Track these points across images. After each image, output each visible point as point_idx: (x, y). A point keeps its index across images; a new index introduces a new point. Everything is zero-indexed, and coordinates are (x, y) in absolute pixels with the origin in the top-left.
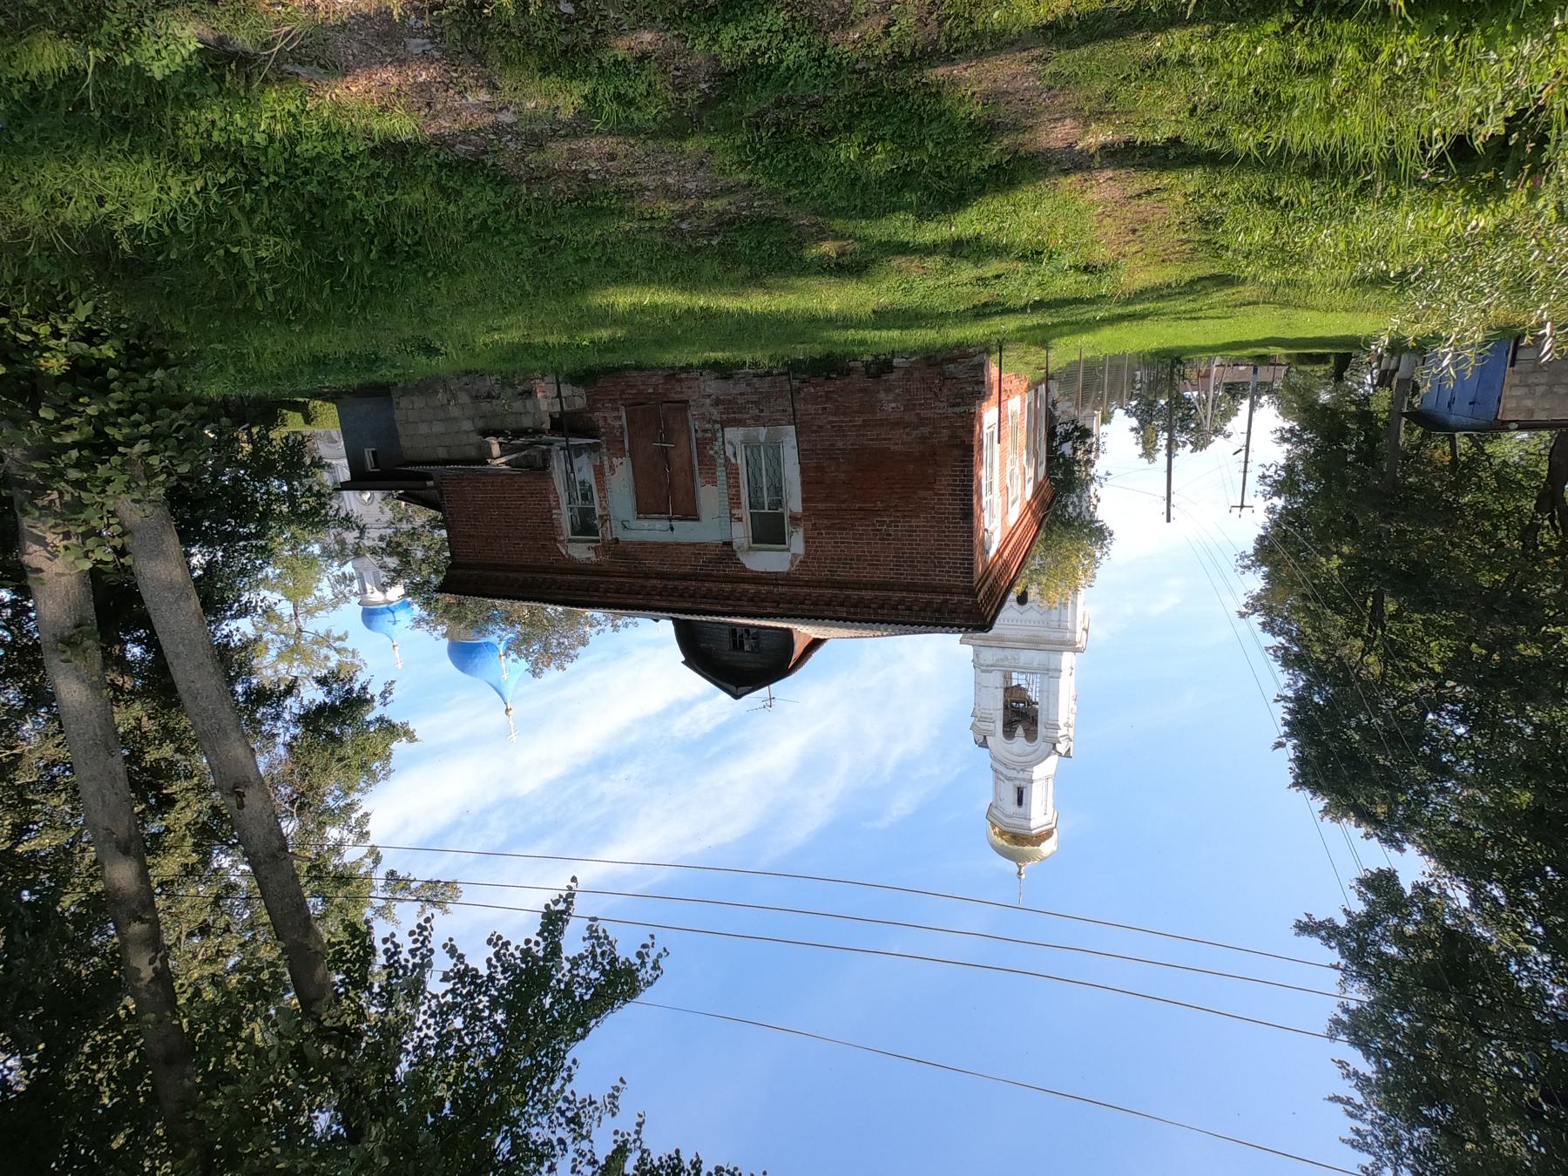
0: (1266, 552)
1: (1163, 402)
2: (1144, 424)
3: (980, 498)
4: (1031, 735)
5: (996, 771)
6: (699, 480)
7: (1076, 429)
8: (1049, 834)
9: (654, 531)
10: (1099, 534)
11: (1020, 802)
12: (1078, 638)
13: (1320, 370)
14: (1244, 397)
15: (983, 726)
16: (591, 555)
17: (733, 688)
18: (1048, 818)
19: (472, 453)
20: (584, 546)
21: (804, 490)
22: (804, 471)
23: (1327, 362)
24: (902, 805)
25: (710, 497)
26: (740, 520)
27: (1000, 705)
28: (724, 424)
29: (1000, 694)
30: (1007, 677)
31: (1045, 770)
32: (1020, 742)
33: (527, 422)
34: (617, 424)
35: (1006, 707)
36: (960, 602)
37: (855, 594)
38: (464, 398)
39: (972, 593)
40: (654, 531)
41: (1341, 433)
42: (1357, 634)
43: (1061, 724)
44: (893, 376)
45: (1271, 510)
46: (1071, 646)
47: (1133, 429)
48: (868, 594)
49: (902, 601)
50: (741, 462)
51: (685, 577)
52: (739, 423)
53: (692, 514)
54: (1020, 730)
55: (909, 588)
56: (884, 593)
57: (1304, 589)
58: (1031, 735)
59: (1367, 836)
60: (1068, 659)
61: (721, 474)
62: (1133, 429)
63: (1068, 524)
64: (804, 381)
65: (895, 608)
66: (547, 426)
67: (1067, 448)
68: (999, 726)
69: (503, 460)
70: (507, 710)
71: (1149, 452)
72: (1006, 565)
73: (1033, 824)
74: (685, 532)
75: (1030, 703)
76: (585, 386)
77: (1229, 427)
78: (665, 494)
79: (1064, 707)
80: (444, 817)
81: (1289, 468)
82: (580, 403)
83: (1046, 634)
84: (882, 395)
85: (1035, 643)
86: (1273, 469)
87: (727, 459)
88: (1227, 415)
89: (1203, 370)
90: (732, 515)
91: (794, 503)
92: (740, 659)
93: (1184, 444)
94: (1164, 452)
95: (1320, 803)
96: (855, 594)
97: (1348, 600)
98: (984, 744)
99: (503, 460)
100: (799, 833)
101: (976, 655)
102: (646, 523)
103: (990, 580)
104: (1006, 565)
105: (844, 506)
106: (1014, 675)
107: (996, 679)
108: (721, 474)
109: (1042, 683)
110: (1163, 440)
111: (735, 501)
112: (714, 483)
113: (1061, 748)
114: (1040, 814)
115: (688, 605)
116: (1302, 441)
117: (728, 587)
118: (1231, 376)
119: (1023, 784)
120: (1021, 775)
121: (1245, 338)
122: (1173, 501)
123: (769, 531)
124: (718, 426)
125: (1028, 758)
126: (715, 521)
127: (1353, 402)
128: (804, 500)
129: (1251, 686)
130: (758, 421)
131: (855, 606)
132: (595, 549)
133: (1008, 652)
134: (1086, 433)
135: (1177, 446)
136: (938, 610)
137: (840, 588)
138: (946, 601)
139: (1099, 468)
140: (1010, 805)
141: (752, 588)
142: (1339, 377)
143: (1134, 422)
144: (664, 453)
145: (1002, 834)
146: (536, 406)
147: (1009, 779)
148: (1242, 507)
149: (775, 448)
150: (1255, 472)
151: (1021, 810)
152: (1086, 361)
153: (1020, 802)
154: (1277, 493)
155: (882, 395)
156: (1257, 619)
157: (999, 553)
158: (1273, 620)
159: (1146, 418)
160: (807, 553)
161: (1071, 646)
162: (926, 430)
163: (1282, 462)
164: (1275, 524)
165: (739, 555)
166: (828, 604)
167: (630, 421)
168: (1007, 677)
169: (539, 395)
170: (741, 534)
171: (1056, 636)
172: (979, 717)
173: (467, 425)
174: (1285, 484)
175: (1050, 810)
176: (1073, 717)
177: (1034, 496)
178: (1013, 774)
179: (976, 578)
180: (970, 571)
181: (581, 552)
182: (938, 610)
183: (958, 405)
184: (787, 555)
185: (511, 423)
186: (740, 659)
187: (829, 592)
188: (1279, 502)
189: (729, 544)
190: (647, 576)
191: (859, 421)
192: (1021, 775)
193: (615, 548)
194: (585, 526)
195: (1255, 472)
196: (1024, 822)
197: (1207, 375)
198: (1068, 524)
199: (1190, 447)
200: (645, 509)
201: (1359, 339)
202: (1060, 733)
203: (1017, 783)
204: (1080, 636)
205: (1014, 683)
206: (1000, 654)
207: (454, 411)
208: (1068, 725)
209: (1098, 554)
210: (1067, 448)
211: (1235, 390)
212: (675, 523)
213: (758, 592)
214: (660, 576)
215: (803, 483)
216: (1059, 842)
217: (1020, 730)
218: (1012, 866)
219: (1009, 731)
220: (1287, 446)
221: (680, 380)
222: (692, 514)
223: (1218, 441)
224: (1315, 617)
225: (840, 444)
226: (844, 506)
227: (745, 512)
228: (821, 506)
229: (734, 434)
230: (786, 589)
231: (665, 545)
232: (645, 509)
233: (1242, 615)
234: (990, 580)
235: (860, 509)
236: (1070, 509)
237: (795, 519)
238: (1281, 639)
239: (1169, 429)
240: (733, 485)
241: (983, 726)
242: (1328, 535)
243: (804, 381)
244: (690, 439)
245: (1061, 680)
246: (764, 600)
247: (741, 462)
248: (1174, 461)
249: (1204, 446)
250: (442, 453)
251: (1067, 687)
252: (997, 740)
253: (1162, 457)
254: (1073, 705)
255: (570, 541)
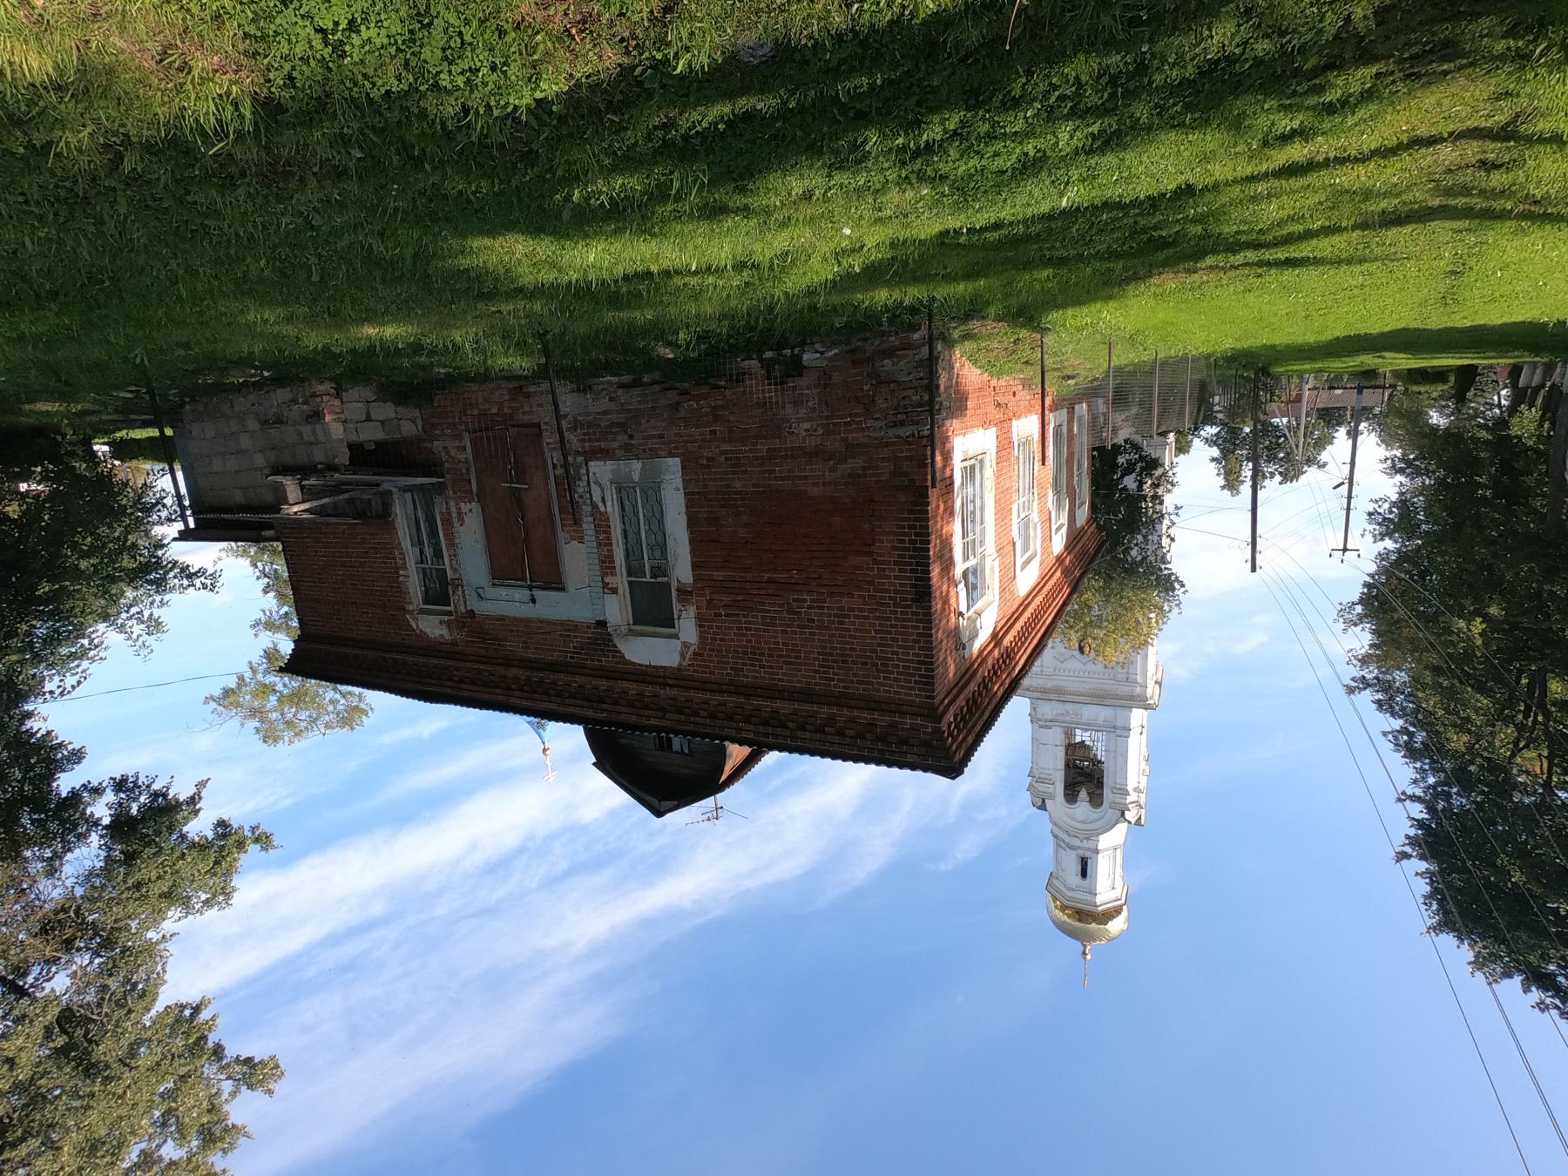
0: (1380, 603)
1: (1247, 430)
2: (1226, 453)
3: (948, 564)
4: (1096, 800)
5: (1056, 837)
6: (562, 536)
7: (1142, 458)
8: (1117, 911)
9: (511, 602)
10: (1167, 584)
11: (1084, 874)
12: (1149, 692)
13: (1436, 390)
14: (1339, 424)
15: (1041, 787)
16: (444, 631)
17: (654, 801)
18: (1117, 893)
19: (269, 497)
20: (436, 619)
21: (693, 551)
22: (692, 523)
23: (1445, 381)
24: (967, 847)
25: (576, 558)
26: (615, 591)
27: (1061, 765)
28: (590, 455)
29: (1061, 752)
30: (1069, 733)
31: (1114, 838)
32: (1083, 807)
33: (319, 456)
34: (462, 457)
35: (1067, 765)
36: (914, 728)
37: (765, 705)
38: (253, 425)
39: (934, 714)
40: (511, 602)
41: (1474, 465)
42: (1508, 720)
43: (1130, 788)
44: (803, 382)
45: (1381, 557)
46: (1142, 702)
47: (1213, 460)
48: (785, 707)
49: (831, 719)
50: (612, 508)
51: (553, 667)
52: (606, 454)
53: (554, 582)
54: (1083, 794)
55: (838, 700)
56: (807, 707)
57: (1433, 658)
58: (1096, 800)
59: (1542, 1007)
60: (1137, 716)
61: (588, 527)
62: (1213, 460)
63: (1131, 570)
64: (685, 392)
65: (820, 730)
66: (343, 458)
67: (1130, 482)
68: (1060, 788)
69: (306, 506)
70: (545, 750)
71: (1232, 484)
72: (1008, 655)
73: (1099, 900)
74: (550, 606)
75: (1097, 763)
76: (419, 406)
77: (1324, 456)
78: (526, 557)
79: (1135, 771)
80: (510, 841)
81: (1403, 504)
82: (409, 429)
83: (1112, 687)
84: (789, 410)
85: (1100, 698)
86: (1386, 506)
87: (594, 505)
88: (1323, 442)
89: (1294, 394)
90: (605, 585)
91: (682, 571)
92: (664, 759)
93: (1272, 475)
94: (1249, 483)
95: (1466, 953)
96: (765, 705)
97: (1498, 679)
98: (1043, 807)
99: (306, 506)
100: (860, 872)
101: (1034, 708)
102: (503, 592)
103: (973, 687)
104: (1008, 655)
105: (749, 576)
106: (1078, 732)
107: (1056, 737)
108: (588, 527)
109: (1108, 740)
110: (1247, 472)
111: (607, 565)
112: (581, 540)
113: (1129, 815)
114: (1108, 886)
115: (553, 707)
116: (1418, 472)
117: (604, 684)
118: (1325, 399)
119: (1087, 854)
120: (1085, 844)
121: (1363, 329)
122: (1259, 531)
123: (653, 611)
124: (580, 459)
125: (1093, 826)
126: (585, 596)
127: (1485, 427)
128: (695, 566)
129: (1365, 783)
130: (630, 452)
131: (765, 723)
132: (448, 624)
133: (1069, 707)
134: (1155, 463)
135: (1264, 477)
136: (882, 738)
137: (748, 696)
138: (893, 725)
139: (1169, 501)
140: (1073, 877)
141: (633, 688)
142: (1460, 397)
143: (1215, 452)
144: (516, 497)
145: (1063, 908)
146: (327, 432)
147: (1072, 848)
148: (1345, 550)
149: (653, 490)
150: (1362, 505)
151: (1085, 883)
152: (1119, 369)
153: (1084, 874)
154: (1388, 534)
155: (789, 410)
156: (1367, 698)
157: (996, 638)
158: (1392, 698)
159: (1228, 447)
160: (702, 637)
161: (1142, 702)
162: (857, 464)
163: (1394, 497)
164: (1383, 571)
165: (616, 641)
166: (730, 718)
167: (476, 454)
168: (1069, 733)
169: (328, 418)
170: (616, 611)
171: (1123, 690)
172: (1037, 779)
173: (259, 460)
174: (1399, 521)
175: (1119, 883)
176: (1144, 780)
177: (1069, 547)
178: (1076, 842)
179: (940, 689)
180: (928, 681)
181: (433, 627)
182: (882, 738)
183: (902, 424)
184: (676, 644)
185: (301, 456)
186: (664, 759)
187: (732, 700)
188: (1389, 544)
189: (602, 624)
190: (508, 662)
191: (763, 448)
192: (1085, 844)
193: (469, 621)
194: (439, 592)
195: (1362, 505)
196: (1089, 897)
197: (1299, 399)
198: (1131, 570)
199: (1278, 478)
200: (502, 574)
201: (228, 873)
202: (1129, 799)
203: (1081, 852)
204: (1152, 690)
205: (1078, 739)
206: (1061, 708)
207: (245, 442)
208: (1138, 790)
209: (1166, 608)
210: (1130, 482)
211: (1330, 417)
212: (537, 593)
213: (641, 694)
214: (525, 663)
215: (692, 542)
216: (1129, 920)
217: (1083, 794)
218: (1077, 945)
219: (1071, 794)
220: (1399, 478)
221: (528, 395)
222: (554, 582)
223: (1312, 473)
224: (1449, 695)
225: (738, 485)
226: (749, 576)
227: (621, 580)
228: (719, 575)
229: (601, 470)
230: (675, 692)
231: (526, 621)
232: (502, 574)
233: (1351, 691)
234: (973, 687)
235: (770, 581)
236: (1134, 553)
237: (684, 593)
238: (1401, 722)
239: (1254, 458)
240: (605, 543)
241: (1041, 787)
242: (1468, 588)
243: (685, 392)
244: (547, 478)
245: (1130, 740)
246: (646, 707)
247: (612, 508)
248: (1260, 494)
249: (1296, 477)
250: (239, 497)
251: (1136, 746)
252: (1058, 803)
253: (1246, 489)
254: (1143, 763)
255: (422, 612)
